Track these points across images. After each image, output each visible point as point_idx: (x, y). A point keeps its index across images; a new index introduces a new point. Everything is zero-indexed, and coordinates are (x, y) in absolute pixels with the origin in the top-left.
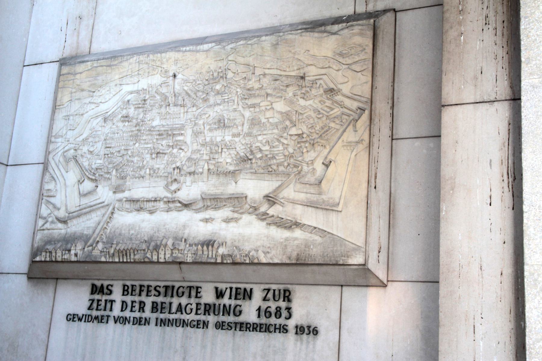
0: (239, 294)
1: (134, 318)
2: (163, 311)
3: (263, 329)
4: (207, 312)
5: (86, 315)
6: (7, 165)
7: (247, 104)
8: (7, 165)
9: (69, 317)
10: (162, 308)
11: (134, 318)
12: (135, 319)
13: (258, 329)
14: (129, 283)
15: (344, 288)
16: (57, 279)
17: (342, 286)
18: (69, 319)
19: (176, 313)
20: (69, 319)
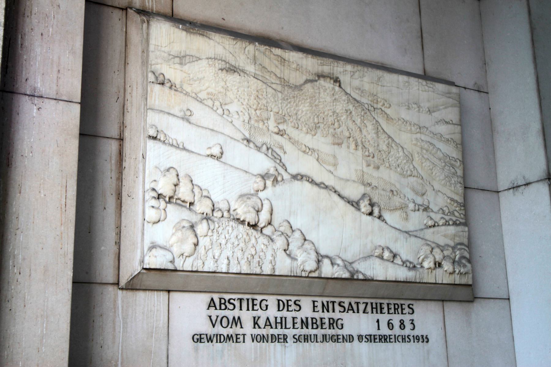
0: (256, 305)
1: (272, 335)
2: (324, 327)
3: (393, 340)
4: (331, 325)
5: (217, 335)
6: (498, 192)
7: (378, 145)
8: (498, 192)
9: (196, 337)
10: (322, 324)
11: (272, 335)
12: (273, 336)
13: (388, 340)
14: (284, 298)
15: (172, 294)
16: (169, 291)
17: (169, 291)
18: (195, 340)
19: (264, 328)
20: (195, 340)
